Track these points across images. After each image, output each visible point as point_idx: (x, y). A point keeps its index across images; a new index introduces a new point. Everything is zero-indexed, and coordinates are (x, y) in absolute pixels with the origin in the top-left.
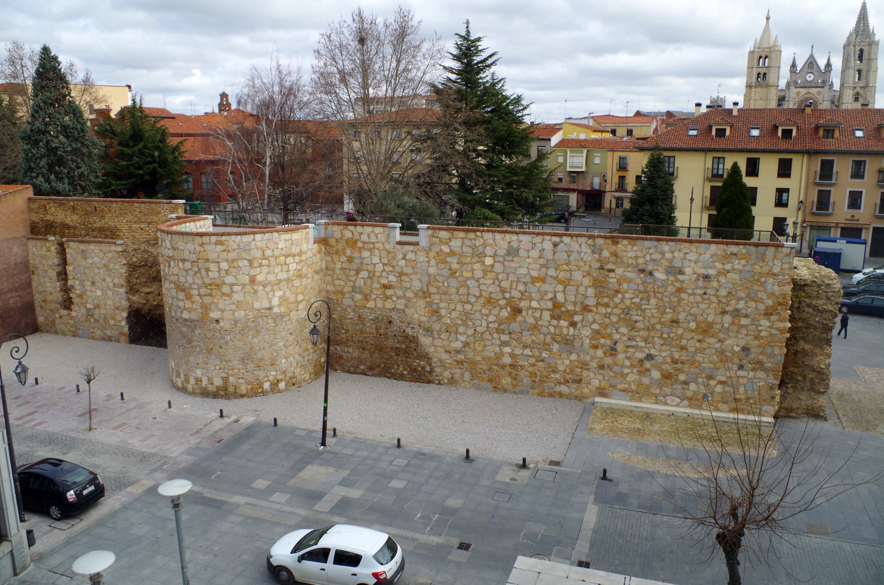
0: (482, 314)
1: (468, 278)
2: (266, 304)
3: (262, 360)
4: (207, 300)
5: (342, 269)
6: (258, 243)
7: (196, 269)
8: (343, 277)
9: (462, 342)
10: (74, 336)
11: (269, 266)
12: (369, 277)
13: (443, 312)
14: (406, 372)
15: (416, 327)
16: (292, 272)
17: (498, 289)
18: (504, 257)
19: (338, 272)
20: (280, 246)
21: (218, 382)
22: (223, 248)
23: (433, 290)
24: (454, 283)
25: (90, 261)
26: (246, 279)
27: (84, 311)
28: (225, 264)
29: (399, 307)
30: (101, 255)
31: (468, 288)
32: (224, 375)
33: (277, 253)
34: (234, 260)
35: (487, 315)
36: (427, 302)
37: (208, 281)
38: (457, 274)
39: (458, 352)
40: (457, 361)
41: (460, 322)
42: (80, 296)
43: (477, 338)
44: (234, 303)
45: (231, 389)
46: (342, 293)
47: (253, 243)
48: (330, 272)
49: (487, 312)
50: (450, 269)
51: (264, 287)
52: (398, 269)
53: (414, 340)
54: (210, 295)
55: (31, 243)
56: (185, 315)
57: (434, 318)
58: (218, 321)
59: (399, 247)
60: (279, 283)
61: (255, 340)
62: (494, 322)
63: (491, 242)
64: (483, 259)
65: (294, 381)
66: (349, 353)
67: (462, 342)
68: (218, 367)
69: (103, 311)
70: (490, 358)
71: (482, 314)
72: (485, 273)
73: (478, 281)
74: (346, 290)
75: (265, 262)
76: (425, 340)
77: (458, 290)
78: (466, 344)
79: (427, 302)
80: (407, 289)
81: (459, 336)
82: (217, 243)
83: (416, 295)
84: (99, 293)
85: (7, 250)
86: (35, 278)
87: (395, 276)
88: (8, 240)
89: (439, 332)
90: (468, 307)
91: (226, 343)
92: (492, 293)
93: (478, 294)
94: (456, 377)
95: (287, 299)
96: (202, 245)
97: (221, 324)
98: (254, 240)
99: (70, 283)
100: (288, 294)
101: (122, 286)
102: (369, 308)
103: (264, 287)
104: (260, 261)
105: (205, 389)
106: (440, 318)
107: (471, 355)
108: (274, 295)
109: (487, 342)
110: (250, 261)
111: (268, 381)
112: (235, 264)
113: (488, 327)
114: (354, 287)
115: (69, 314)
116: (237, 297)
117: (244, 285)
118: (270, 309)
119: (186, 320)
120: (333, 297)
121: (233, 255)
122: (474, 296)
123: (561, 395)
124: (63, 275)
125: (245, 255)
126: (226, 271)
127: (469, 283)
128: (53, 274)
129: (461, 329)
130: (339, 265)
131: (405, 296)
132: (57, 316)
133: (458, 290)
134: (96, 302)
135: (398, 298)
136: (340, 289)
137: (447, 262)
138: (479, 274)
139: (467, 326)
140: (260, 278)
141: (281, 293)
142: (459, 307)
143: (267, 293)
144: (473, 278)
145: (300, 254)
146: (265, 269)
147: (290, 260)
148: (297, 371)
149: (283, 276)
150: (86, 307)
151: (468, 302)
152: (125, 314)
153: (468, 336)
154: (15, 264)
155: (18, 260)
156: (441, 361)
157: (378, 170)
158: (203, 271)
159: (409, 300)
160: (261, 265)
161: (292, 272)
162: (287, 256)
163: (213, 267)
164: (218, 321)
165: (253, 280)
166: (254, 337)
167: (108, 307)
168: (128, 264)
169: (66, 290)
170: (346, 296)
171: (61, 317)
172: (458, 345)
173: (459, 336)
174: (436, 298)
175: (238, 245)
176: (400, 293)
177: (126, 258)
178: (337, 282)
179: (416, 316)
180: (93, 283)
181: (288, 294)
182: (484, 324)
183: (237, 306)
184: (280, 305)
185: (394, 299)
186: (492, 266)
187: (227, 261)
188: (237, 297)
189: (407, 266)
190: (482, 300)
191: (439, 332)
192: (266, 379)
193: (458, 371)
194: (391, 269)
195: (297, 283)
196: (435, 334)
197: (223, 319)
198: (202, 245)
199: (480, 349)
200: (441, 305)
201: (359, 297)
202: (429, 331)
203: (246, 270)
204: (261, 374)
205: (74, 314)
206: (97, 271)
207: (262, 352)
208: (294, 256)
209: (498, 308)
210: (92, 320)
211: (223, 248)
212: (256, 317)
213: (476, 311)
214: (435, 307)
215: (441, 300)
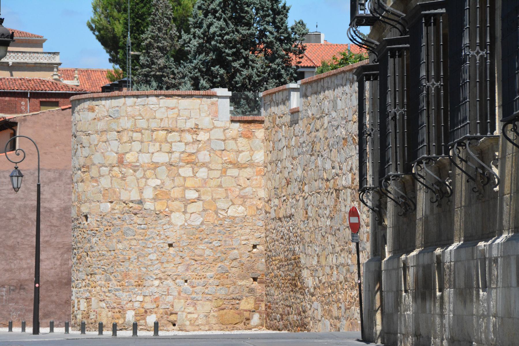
2: (135, 196)
16: (176, 155)
20: (158, 115)
26: (113, 158)
33: (154, 125)
51: (135, 171)
55: (175, 319)
60: (155, 169)
61: (120, 246)
95: (167, 193)
100: (168, 184)
103: (135, 171)
104: (130, 133)
116: (105, 182)
118: (140, 202)
123: (398, 299)
125: (114, 126)
140: (130, 158)
141: (158, 182)
143: (137, 179)
145: (196, 130)
146: (137, 146)
147: (174, 136)
149: (162, 158)
157: (143, 7)
161: (176, 155)
162: (169, 131)
181: (168, 184)
184: (155, 199)
188: (105, 182)
195: (186, 171)
204: (124, 296)
207: (127, 264)
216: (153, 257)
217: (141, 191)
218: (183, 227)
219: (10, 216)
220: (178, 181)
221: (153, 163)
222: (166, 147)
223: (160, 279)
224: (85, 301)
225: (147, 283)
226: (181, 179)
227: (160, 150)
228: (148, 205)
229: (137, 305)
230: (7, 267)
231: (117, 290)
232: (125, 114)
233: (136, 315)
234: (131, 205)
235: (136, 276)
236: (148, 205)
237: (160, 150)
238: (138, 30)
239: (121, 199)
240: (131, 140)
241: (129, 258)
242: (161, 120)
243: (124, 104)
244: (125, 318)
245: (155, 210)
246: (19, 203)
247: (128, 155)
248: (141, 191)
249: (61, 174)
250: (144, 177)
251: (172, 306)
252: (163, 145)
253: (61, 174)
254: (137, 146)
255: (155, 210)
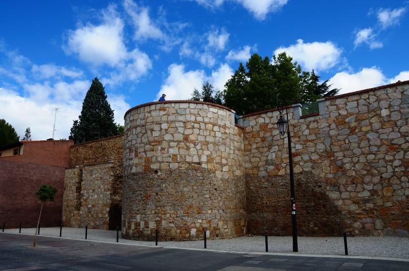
0: (386, 161)
1: (367, 133)
2: (196, 160)
3: (191, 207)
4: (149, 154)
5: (257, 148)
6: (192, 111)
7: (144, 131)
8: (258, 155)
9: (369, 191)
10: (79, 227)
11: (200, 129)
12: (279, 151)
13: (347, 166)
14: (317, 228)
15: (323, 185)
17: (399, 135)
18: (399, 105)
19: (254, 151)
21: (152, 225)
22: (165, 113)
23: (336, 148)
24: (354, 139)
25: (94, 176)
27: (86, 210)
28: (166, 124)
29: (306, 170)
30: (100, 171)
31: (369, 140)
32: (158, 219)
33: (206, 120)
34: (172, 122)
35: (392, 161)
36: (331, 161)
37: (151, 139)
38: (357, 130)
39: (366, 201)
40: (364, 210)
41: (365, 172)
42: (86, 200)
43: (385, 185)
44: (170, 157)
45: (163, 232)
46: (257, 167)
47: (188, 110)
48: (247, 153)
49: (391, 158)
50: (349, 128)
52: (303, 138)
53: (324, 197)
54: (153, 150)
56: (134, 170)
57: (340, 173)
58: (156, 172)
59: (302, 120)
61: (185, 189)
62: (400, 166)
63: (384, 96)
64: (378, 112)
65: (218, 232)
66: (263, 217)
67: (369, 191)
68: (153, 212)
69: (96, 209)
70: (400, 202)
71: (386, 161)
72: (383, 123)
73: (377, 132)
74: (260, 164)
75: (196, 125)
76: (333, 195)
77: (359, 144)
78: (373, 192)
79: (331, 161)
80: (312, 153)
81: (365, 186)
82: (160, 110)
83: (321, 156)
84: (96, 196)
85: (52, 172)
86: (65, 192)
87: (301, 144)
88: (54, 166)
89: (346, 185)
90: (371, 157)
91: (162, 190)
92: (393, 139)
93: (378, 143)
94: (368, 226)
96: (149, 112)
97: (159, 173)
98: (189, 107)
99: (82, 192)
101: (109, 190)
102: (281, 176)
104: (193, 124)
105: (142, 232)
106: (344, 172)
107: (380, 202)
108: (203, 153)
109: (395, 187)
110: (184, 123)
111: (195, 227)
112: (173, 125)
113: (394, 172)
114: (267, 161)
115: (78, 213)
117: (179, 142)
118: (199, 163)
119: (134, 174)
120: (251, 172)
121: (171, 118)
122: (376, 146)
124: (79, 189)
126: (166, 130)
127: (368, 135)
128: (74, 188)
129: (367, 179)
130: (254, 146)
131: (311, 159)
132: (72, 215)
133: (359, 144)
134: (94, 203)
135: (306, 162)
136: (256, 164)
137: (345, 123)
138: (377, 126)
139: (373, 175)
140: (192, 137)
141: (209, 153)
142: (362, 159)
144: (372, 130)
146: (196, 131)
148: (221, 223)
150: (88, 207)
151: (371, 153)
152: (108, 209)
153: (374, 185)
154: (56, 181)
155: (58, 180)
156: (349, 212)
158: (149, 132)
159: (314, 162)
160: (193, 127)
162: (214, 125)
163: (156, 127)
164: (156, 172)
165: (186, 138)
166: (185, 186)
167: (99, 206)
168: (114, 176)
169: (80, 196)
170: (262, 169)
171: (74, 216)
172: (366, 194)
173: (365, 186)
174: (340, 155)
175: (176, 111)
176: (306, 157)
177: (113, 172)
178: (253, 160)
179: (322, 175)
180: (94, 191)
182: (390, 169)
183: (172, 159)
184: (207, 162)
185: (301, 164)
186: (389, 116)
187: (167, 122)
189: (310, 134)
190: (383, 149)
191: (346, 185)
192: (193, 225)
193: (368, 220)
194: (298, 139)
196: (342, 188)
197: (160, 170)
198: (149, 112)
199: (389, 194)
200: (345, 160)
201: (272, 167)
202: (336, 186)
203: (181, 130)
204: (189, 220)
205: (81, 212)
206: (96, 182)
207: (191, 200)
208: (220, 126)
209: (402, 152)
210: (90, 216)
211: (165, 113)
212: (187, 169)
213: (379, 159)
214: (339, 163)
215: (344, 156)
216: (207, 196)
217: (200, 157)
218: (222, 180)
219: (16, 181)
220: (219, 153)
221: (206, 141)
222: (212, 133)
223: (211, 209)
224: (155, 222)
225: (204, 212)
226: (220, 152)
227: (210, 135)
228: (204, 166)
229: (198, 225)
230: (12, 203)
231: (184, 216)
232: (189, 113)
233: (197, 231)
234: (193, 165)
235: (197, 207)
236: (204, 166)
237: (210, 135)
238: (89, 110)
239: (187, 161)
240: (193, 127)
241: (193, 197)
242: (210, 118)
243: (189, 107)
244: (190, 233)
245: (208, 168)
246: (20, 176)
247: (190, 136)
248: (200, 157)
249: (38, 167)
250: (201, 149)
251: (218, 225)
252: (211, 132)
253: (38, 167)
254: (196, 131)
255: (208, 168)
